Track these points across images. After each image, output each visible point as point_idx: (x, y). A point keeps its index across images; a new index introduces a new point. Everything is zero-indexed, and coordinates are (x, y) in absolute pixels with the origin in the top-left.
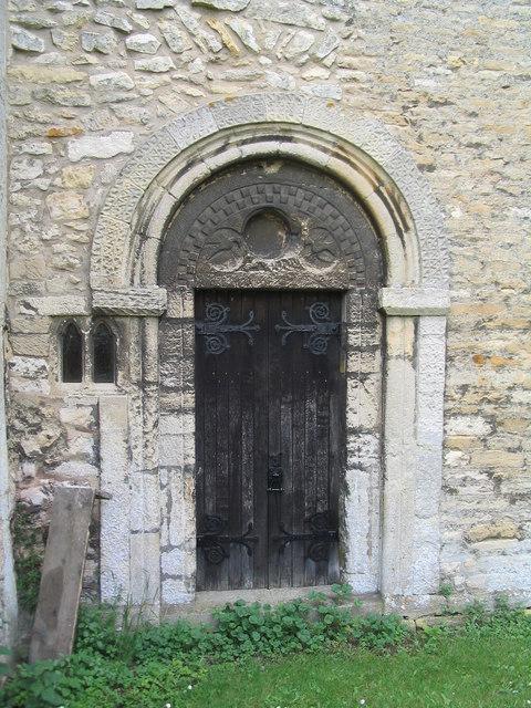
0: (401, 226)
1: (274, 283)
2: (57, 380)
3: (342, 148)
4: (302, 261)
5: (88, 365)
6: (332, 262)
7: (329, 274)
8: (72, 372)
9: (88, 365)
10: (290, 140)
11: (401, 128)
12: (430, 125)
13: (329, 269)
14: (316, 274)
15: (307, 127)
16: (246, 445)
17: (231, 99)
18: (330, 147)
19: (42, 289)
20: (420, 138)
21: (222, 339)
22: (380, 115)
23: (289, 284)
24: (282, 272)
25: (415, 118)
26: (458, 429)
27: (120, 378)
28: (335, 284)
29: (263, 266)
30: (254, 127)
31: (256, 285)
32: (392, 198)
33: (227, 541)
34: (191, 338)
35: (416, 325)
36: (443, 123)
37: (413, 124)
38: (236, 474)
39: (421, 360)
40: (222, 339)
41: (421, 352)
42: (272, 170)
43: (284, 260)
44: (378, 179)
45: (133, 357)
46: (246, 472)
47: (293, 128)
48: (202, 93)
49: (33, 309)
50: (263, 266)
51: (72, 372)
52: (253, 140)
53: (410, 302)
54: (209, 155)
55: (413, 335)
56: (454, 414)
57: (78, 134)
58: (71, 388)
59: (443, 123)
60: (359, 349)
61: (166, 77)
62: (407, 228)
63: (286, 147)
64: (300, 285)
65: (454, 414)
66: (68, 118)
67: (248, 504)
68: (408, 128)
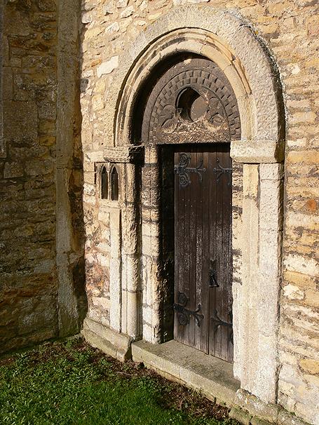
4: (206, 123)
5: (110, 190)
7: (218, 131)
8: (104, 196)
9: (110, 190)
10: (183, 39)
11: (252, 8)
13: (218, 128)
14: (212, 132)
15: (190, 28)
16: (199, 251)
18: (203, 38)
20: (267, 12)
24: (193, 132)
26: (295, 266)
28: (222, 139)
29: (184, 128)
33: (190, 312)
38: (193, 268)
42: (188, 61)
46: (199, 270)
47: (183, 30)
50: (184, 128)
51: (104, 196)
52: (167, 45)
56: (292, 252)
57: (101, 62)
58: (103, 202)
64: (204, 141)
65: (292, 252)
67: (199, 291)
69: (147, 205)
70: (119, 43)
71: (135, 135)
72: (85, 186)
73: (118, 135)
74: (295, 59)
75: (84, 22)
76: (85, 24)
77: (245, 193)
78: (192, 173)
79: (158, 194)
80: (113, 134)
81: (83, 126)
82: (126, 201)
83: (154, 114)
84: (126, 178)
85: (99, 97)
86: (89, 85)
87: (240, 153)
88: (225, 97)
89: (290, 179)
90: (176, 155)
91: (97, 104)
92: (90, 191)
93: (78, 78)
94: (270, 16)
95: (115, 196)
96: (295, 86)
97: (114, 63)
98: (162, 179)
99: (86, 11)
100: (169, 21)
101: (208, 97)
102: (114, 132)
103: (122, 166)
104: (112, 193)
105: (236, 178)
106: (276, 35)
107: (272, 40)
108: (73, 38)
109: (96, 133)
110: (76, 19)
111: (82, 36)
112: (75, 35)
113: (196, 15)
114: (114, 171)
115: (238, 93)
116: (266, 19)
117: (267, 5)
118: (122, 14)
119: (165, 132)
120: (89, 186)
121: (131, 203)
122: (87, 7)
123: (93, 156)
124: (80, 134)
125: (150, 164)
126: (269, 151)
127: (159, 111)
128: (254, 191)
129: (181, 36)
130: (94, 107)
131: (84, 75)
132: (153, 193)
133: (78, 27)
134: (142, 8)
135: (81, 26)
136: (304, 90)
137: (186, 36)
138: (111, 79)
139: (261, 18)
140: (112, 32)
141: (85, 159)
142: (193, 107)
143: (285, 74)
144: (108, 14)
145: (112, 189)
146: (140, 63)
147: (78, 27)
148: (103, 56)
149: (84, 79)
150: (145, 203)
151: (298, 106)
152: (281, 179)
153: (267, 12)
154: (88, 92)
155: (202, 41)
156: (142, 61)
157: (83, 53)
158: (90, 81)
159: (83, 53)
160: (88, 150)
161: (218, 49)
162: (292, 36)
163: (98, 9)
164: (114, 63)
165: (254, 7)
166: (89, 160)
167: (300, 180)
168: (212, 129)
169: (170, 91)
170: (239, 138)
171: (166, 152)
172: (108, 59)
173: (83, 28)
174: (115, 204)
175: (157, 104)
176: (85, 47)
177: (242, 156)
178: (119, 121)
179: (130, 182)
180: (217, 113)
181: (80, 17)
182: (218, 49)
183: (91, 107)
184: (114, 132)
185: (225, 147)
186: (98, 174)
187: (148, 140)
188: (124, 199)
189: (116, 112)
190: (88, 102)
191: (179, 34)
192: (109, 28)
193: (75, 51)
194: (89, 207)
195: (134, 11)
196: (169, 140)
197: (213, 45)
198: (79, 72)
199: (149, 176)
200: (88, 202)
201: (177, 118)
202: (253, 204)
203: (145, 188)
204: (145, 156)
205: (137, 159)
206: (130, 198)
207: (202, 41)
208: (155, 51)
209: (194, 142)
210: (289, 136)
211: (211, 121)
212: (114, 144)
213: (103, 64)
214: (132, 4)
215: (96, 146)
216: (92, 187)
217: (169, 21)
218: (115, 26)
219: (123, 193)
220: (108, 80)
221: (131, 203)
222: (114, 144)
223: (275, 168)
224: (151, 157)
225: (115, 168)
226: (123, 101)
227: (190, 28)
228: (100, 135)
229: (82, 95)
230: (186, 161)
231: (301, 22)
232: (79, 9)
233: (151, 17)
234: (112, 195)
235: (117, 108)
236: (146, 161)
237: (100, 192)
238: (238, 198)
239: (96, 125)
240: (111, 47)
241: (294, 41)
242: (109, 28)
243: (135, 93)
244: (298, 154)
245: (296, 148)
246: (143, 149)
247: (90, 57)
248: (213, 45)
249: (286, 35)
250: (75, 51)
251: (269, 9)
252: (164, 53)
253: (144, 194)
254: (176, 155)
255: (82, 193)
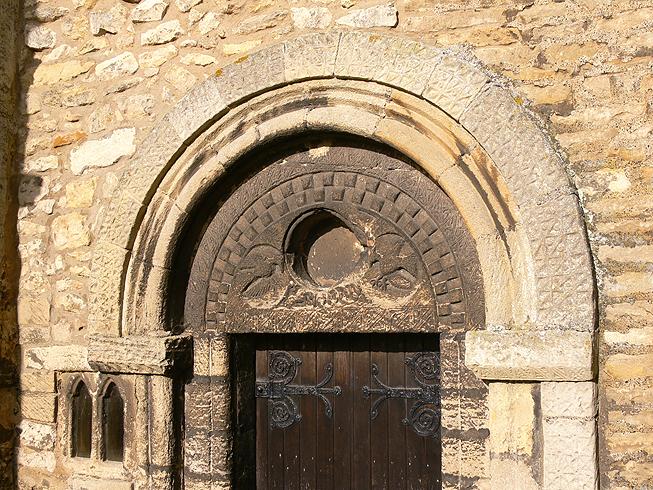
0: (502, 218)
1: (326, 326)
2: (65, 454)
3: (400, 103)
4: (366, 288)
5: (96, 437)
6: (411, 288)
7: (405, 308)
8: (80, 447)
9: (96, 437)
10: (324, 102)
11: (503, 50)
12: (559, 32)
13: (404, 301)
14: (387, 309)
15: (345, 78)
17: (243, 59)
18: (381, 102)
19: (47, 337)
20: (541, 60)
21: (290, 405)
22: (465, 36)
23: (346, 327)
25: (529, 27)
27: (126, 456)
28: (414, 324)
29: (306, 299)
30: (274, 93)
31: (299, 328)
32: (484, 171)
34: (222, 405)
35: (537, 398)
36: (586, 24)
37: (526, 38)
39: (548, 461)
40: (290, 405)
41: (547, 449)
42: (319, 152)
43: (341, 289)
44: (459, 143)
45: (139, 429)
47: (325, 83)
48: (213, 59)
49: (41, 363)
50: (306, 299)
51: (80, 447)
52: (275, 113)
53: (522, 358)
54: (222, 142)
55: (532, 417)
57: (82, 138)
59: (586, 24)
60: (456, 434)
61: (171, 47)
62: (512, 223)
63: (317, 117)
64: (363, 327)
66: (73, 121)
68: (519, 46)
69: (199, 470)
70: (136, 102)
71: (173, 311)
72: (24, 425)
73: (129, 310)
74: (616, 160)
75: (32, 44)
76: (35, 50)
77: (495, 444)
78: (303, 399)
79: (228, 445)
80: (116, 307)
81: (25, 285)
82: (148, 464)
83: (219, 264)
84: (149, 410)
85: (75, 222)
86: (44, 190)
87: (492, 359)
88: (423, 233)
89: (613, 416)
90: (261, 356)
91: (70, 234)
92: (39, 438)
93: (13, 172)
94: (548, 70)
95: (114, 447)
96: (619, 216)
97: (123, 142)
98: (235, 410)
99: (39, 22)
100: (287, 59)
101: (376, 232)
102: (121, 302)
103: (138, 383)
104: (103, 442)
105: (452, 412)
106: (565, 108)
107: (556, 119)
108: (6, 78)
109: (62, 301)
110: (12, 34)
111: (24, 77)
112: (10, 71)
113: (366, 53)
114: (111, 393)
115: (476, 220)
116: (541, 75)
117: (543, 45)
118: (147, 35)
119: (253, 305)
120: (38, 426)
121: (162, 468)
122: (42, 12)
123: (51, 355)
124: (15, 303)
125: (208, 377)
126: (578, 357)
127: (235, 259)
128: (525, 443)
129: (321, 95)
130: (60, 241)
131: (31, 166)
132: (219, 444)
133: (17, 55)
134: (204, 26)
135: (24, 54)
136: (641, 225)
137: (330, 94)
138: (112, 179)
139: (527, 71)
140: (115, 73)
141: (27, 361)
142: (313, 252)
143: (591, 191)
144: (103, 32)
145: (103, 433)
146: (198, 149)
147: (17, 55)
148: (88, 125)
149: (28, 178)
150: (194, 466)
151: (630, 259)
152: (595, 417)
153: (541, 60)
154: (43, 205)
155: (375, 109)
156: (204, 143)
157: (28, 115)
158: (46, 180)
159: (28, 115)
160: (37, 340)
161: (419, 127)
162: (607, 114)
163: (76, 19)
164: (123, 142)
165: (510, 48)
166: (37, 366)
167: (639, 417)
168: (385, 303)
169: (268, 215)
170: (478, 319)
171: (243, 348)
172: (103, 134)
173: (28, 60)
174: (113, 469)
175: (229, 242)
176: (33, 101)
177: (497, 364)
178: (133, 278)
179: (161, 419)
180: (400, 268)
181: (22, 34)
182: (419, 127)
183: (48, 240)
184: (121, 302)
185: (428, 342)
186: (63, 399)
187: (204, 322)
188: (142, 459)
189: (128, 256)
190: (42, 229)
191: (313, 90)
192: (107, 63)
193: (9, 108)
194: (37, 479)
195: (182, 31)
196: (263, 325)
197: (409, 120)
198: (16, 157)
199: (208, 405)
200: (32, 465)
201: (286, 275)
202: (521, 475)
203: (194, 432)
204: (196, 358)
205: (180, 367)
206: (161, 457)
207: (375, 109)
208: (242, 125)
209: (335, 330)
210: (607, 323)
211: (381, 285)
212: (120, 329)
213: (87, 144)
214: (177, 17)
215: (62, 332)
216: (47, 430)
217: (287, 59)
218: (127, 61)
219: (141, 446)
220: (101, 180)
221: (162, 468)
222: (120, 329)
223: (587, 392)
224: (210, 361)
225: (112, 384)
226: (147, 232)
227: (345, 78)
228: (74, 306)
229: (23, 212)
230: (289, 369)
231: (628, 87)
232: (23, 16)
233: (229, 48)
234: (104, 448)
235: (130, 248)
236: (199, 369)
237: (66, 441)
238: (460, 455)
239: (62, 284)
240: (114, 106)
241: (613, 123)
242: (107, 63)
243: (182, 216)
244: (634, 361)
245: (627, 349)
246: (188, 344)
247: (50, 124)
248: (409, 120)
249: (592, 111)
250: (9, 108)
251: (548, 55)
252: (270, 128)
253: (191, 446)
254: (261, 356)
255: (16, 443)
